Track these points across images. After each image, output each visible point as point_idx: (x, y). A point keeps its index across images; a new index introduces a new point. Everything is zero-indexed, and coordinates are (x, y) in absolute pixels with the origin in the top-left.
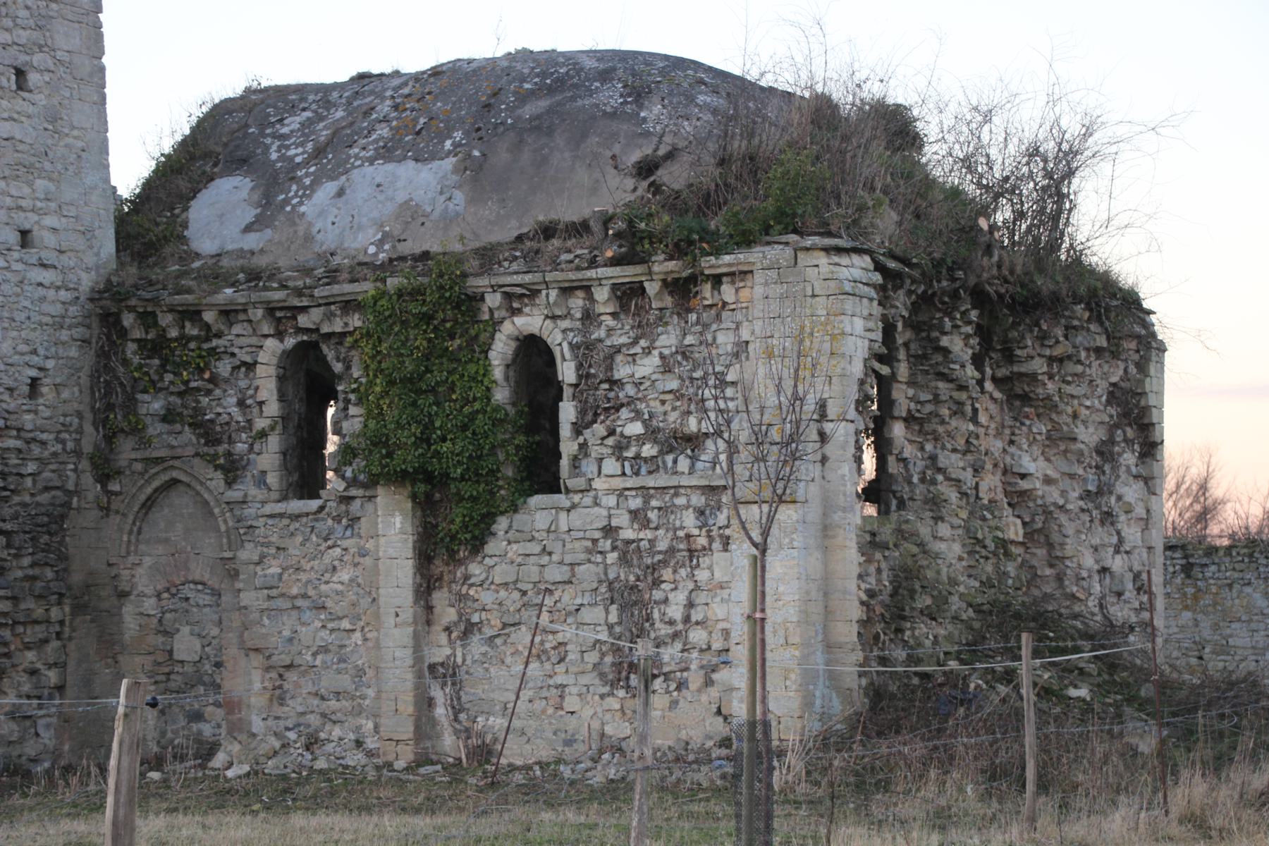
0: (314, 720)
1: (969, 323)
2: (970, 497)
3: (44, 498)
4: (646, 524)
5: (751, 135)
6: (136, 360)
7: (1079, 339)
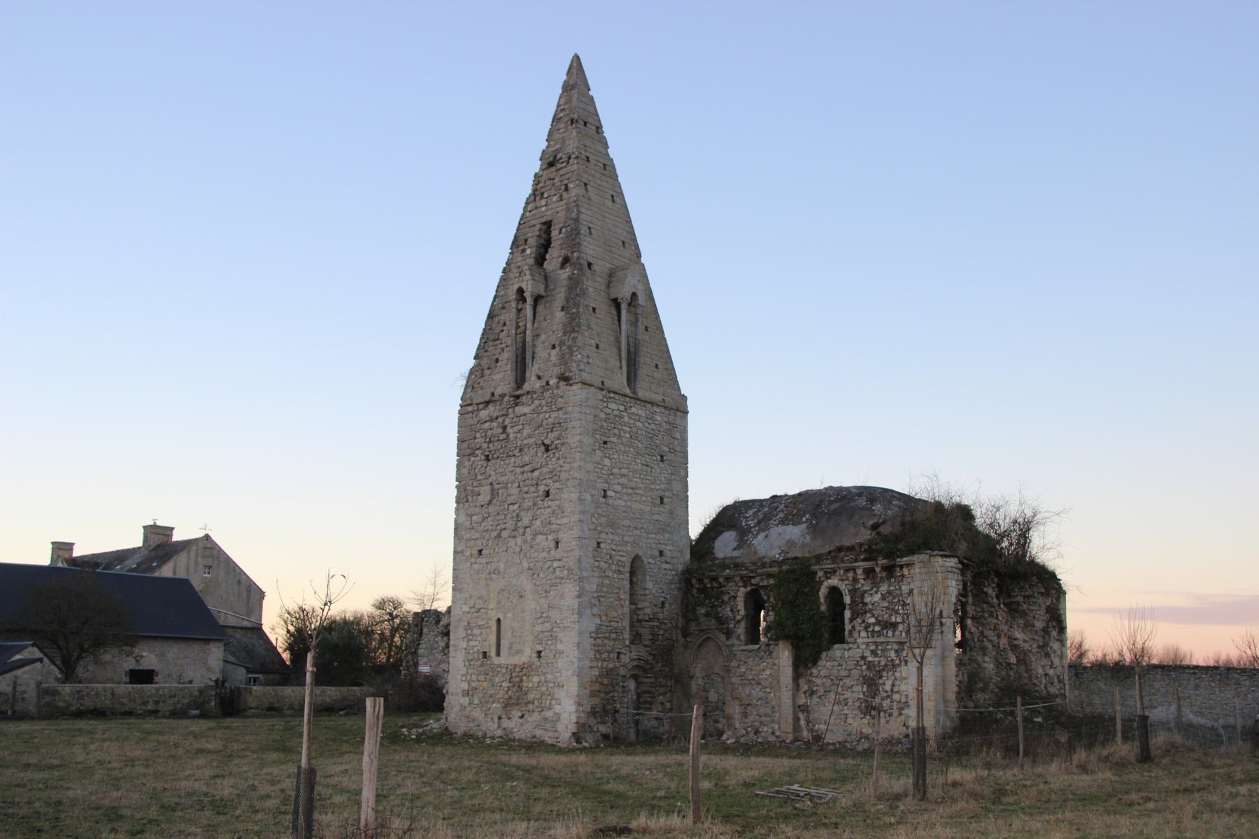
0: (757, 724)
1: (994, 583)
2: (996, 647)
3: (665, 643)
4: (876, 655)
5: (913, 515)
6: (696, 595)
7: (1035, 589)
